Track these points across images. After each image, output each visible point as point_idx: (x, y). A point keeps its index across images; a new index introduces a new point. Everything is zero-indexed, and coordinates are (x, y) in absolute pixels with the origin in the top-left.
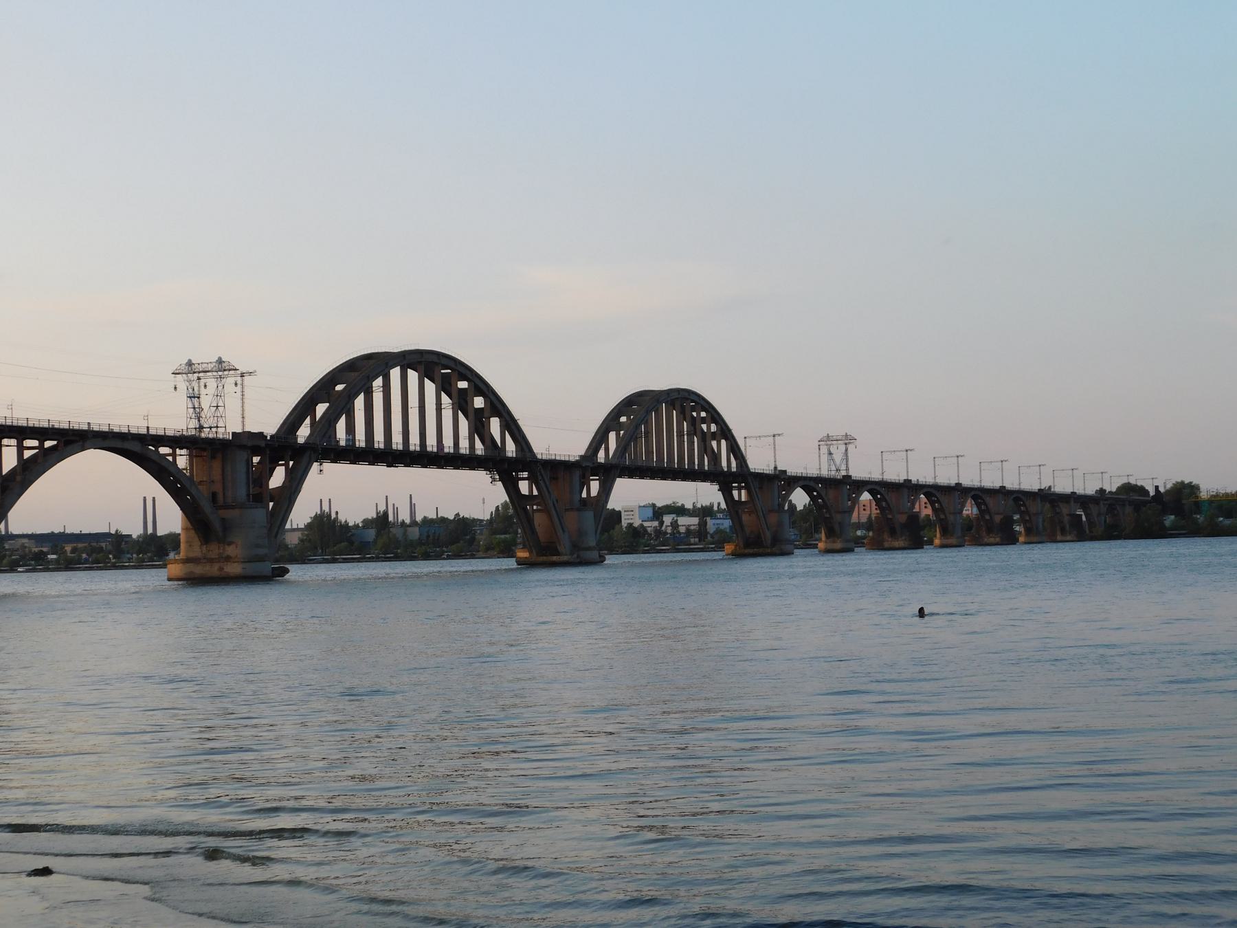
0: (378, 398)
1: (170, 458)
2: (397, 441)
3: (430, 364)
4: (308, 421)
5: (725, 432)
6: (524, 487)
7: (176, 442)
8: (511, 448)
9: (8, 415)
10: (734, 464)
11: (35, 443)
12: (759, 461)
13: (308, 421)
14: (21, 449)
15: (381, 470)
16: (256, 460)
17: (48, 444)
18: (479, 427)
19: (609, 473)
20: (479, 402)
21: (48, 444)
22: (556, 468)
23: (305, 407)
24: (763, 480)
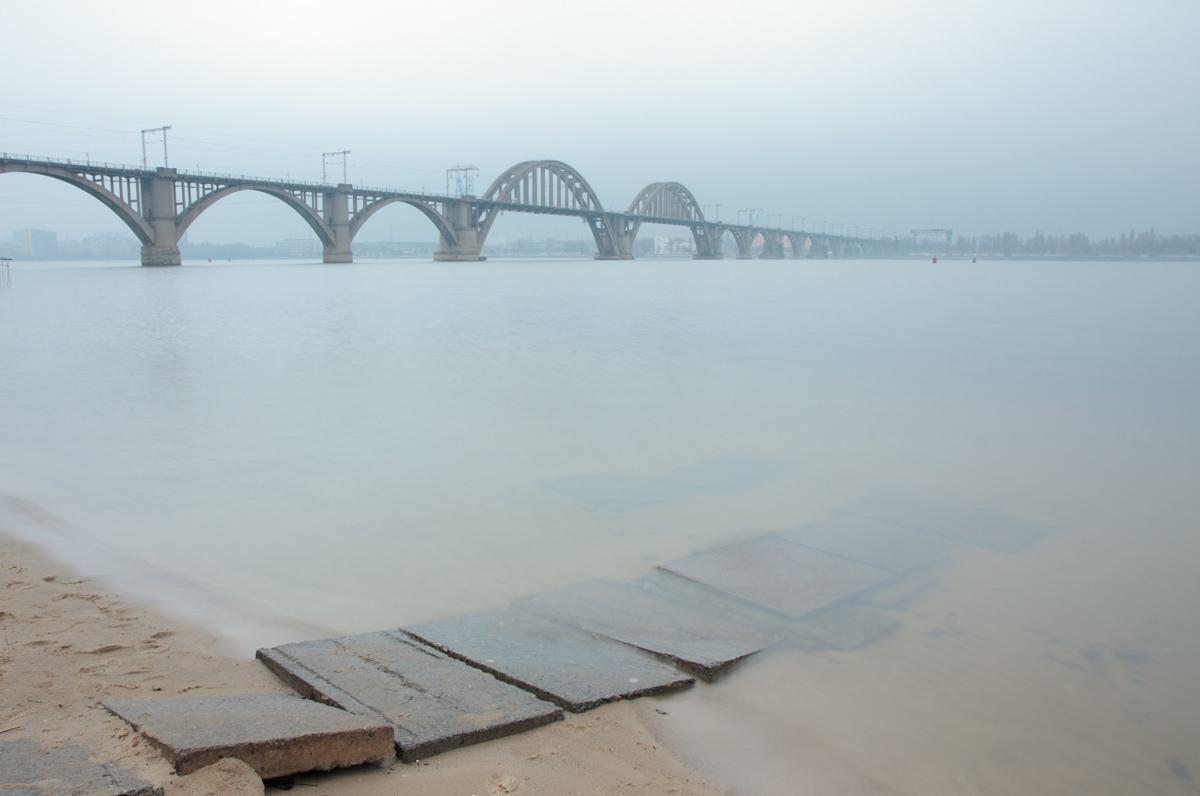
0: (530, 181)
1: (100, 183)
2: (531, 202)
3: (555, 167)
4: (498, 191)
5: (694, 203)
6: (598, 225)
7: (436, 199)
8: (592, 207)
9: (196, 169)
10: (697, 217)
11: (371, 198)
12: (709, 217)
13: (498, 191)
14: (365, 201)
15: (531, 215)
16: (474, 208)
17: (378, 199)
18: (578, 196)
19: (637, 220)
20: (578, 185)
21: (378, 199)
22: (614, 217)
23: (497, 185)
24: (711, 226)
